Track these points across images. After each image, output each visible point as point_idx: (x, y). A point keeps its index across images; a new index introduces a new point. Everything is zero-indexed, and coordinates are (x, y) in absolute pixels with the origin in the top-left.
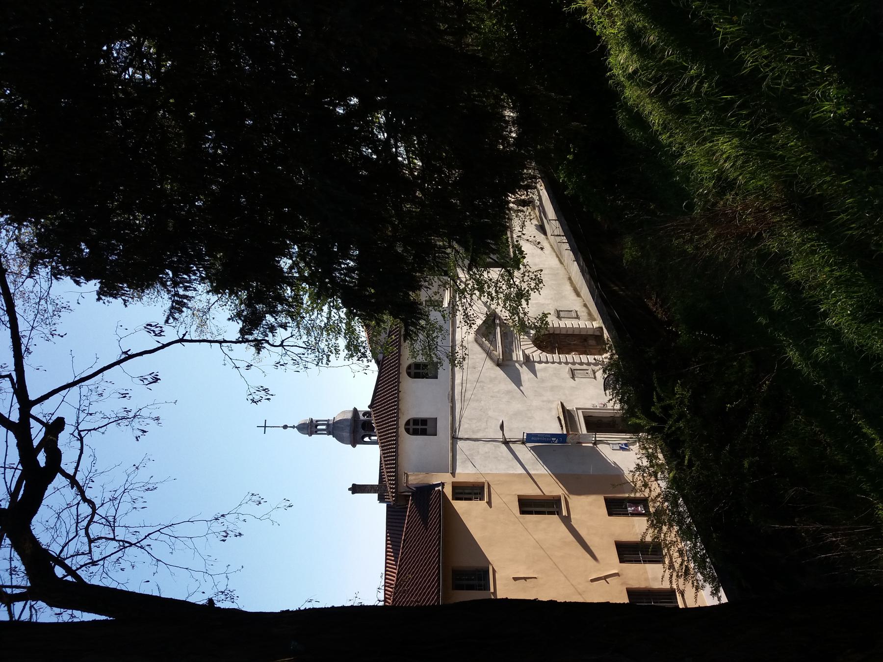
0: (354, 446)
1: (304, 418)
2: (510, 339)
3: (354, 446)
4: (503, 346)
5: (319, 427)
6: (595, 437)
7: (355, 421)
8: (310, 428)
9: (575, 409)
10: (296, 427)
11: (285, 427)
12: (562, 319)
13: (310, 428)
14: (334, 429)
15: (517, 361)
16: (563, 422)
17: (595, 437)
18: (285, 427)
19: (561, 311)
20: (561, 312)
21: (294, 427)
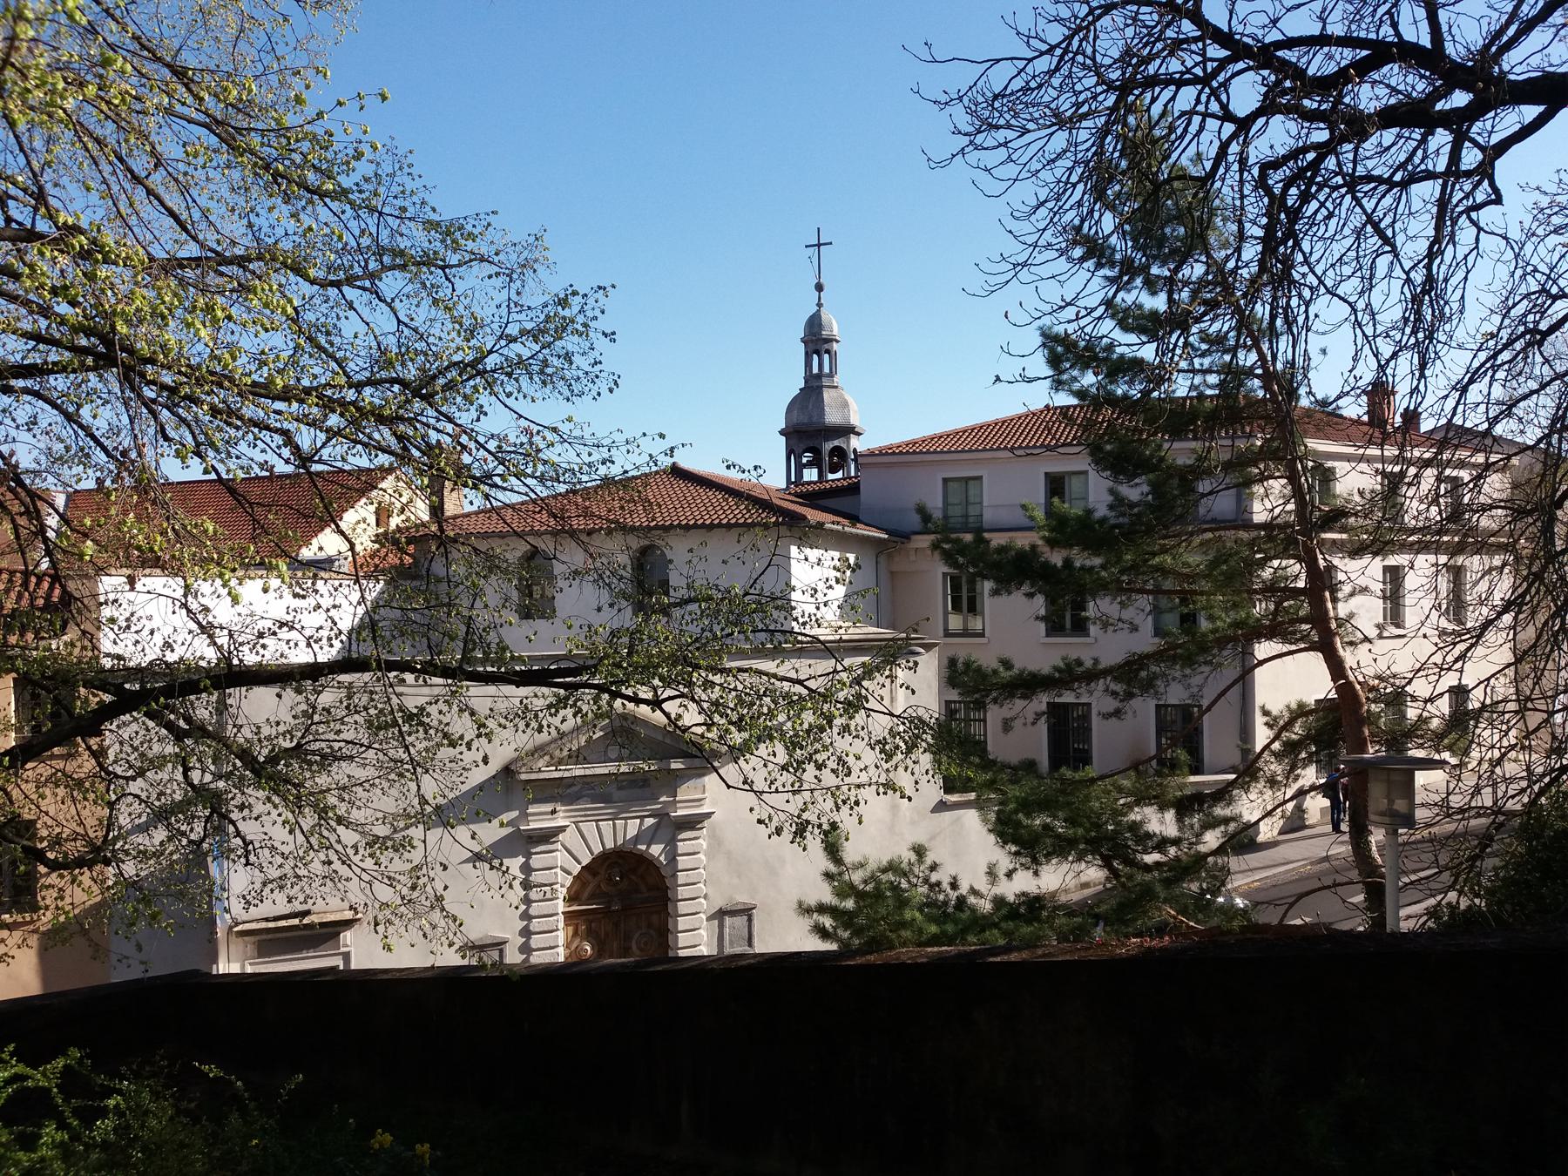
0: (782, 433)
1: (834, 325)
2: (617, 794)
3: (782, 433)
4: (589, 780)
5: (815, 357)
6: (975, 720)
7: (820, 431)
8: (817, 341)
9: (343, 950)
10: (819, 311)
11: (819, 288)
12: (716, 922)
13: (817, 341)
14: (813, 388)
15: (525, 816)
16: (283, 923)
17: (975, 720)
18: (819, 288)
19: (750, 920)
20: (746, 918)
21: (819, 305)
